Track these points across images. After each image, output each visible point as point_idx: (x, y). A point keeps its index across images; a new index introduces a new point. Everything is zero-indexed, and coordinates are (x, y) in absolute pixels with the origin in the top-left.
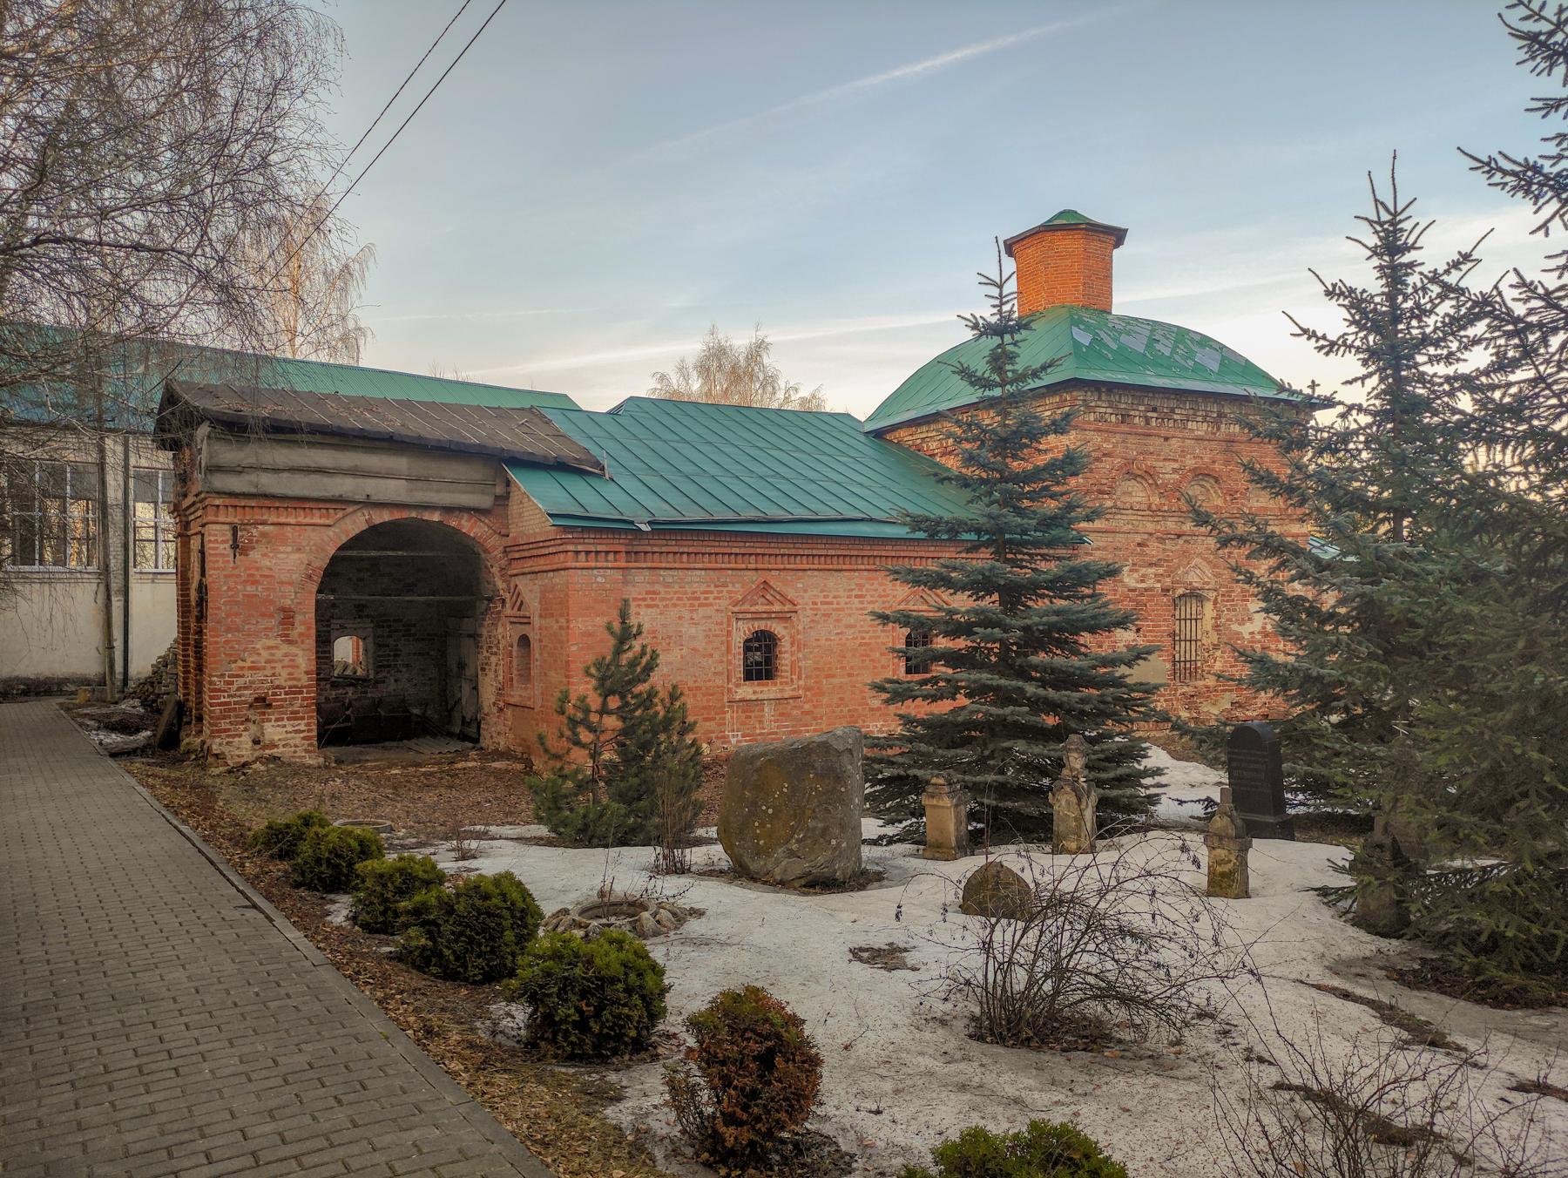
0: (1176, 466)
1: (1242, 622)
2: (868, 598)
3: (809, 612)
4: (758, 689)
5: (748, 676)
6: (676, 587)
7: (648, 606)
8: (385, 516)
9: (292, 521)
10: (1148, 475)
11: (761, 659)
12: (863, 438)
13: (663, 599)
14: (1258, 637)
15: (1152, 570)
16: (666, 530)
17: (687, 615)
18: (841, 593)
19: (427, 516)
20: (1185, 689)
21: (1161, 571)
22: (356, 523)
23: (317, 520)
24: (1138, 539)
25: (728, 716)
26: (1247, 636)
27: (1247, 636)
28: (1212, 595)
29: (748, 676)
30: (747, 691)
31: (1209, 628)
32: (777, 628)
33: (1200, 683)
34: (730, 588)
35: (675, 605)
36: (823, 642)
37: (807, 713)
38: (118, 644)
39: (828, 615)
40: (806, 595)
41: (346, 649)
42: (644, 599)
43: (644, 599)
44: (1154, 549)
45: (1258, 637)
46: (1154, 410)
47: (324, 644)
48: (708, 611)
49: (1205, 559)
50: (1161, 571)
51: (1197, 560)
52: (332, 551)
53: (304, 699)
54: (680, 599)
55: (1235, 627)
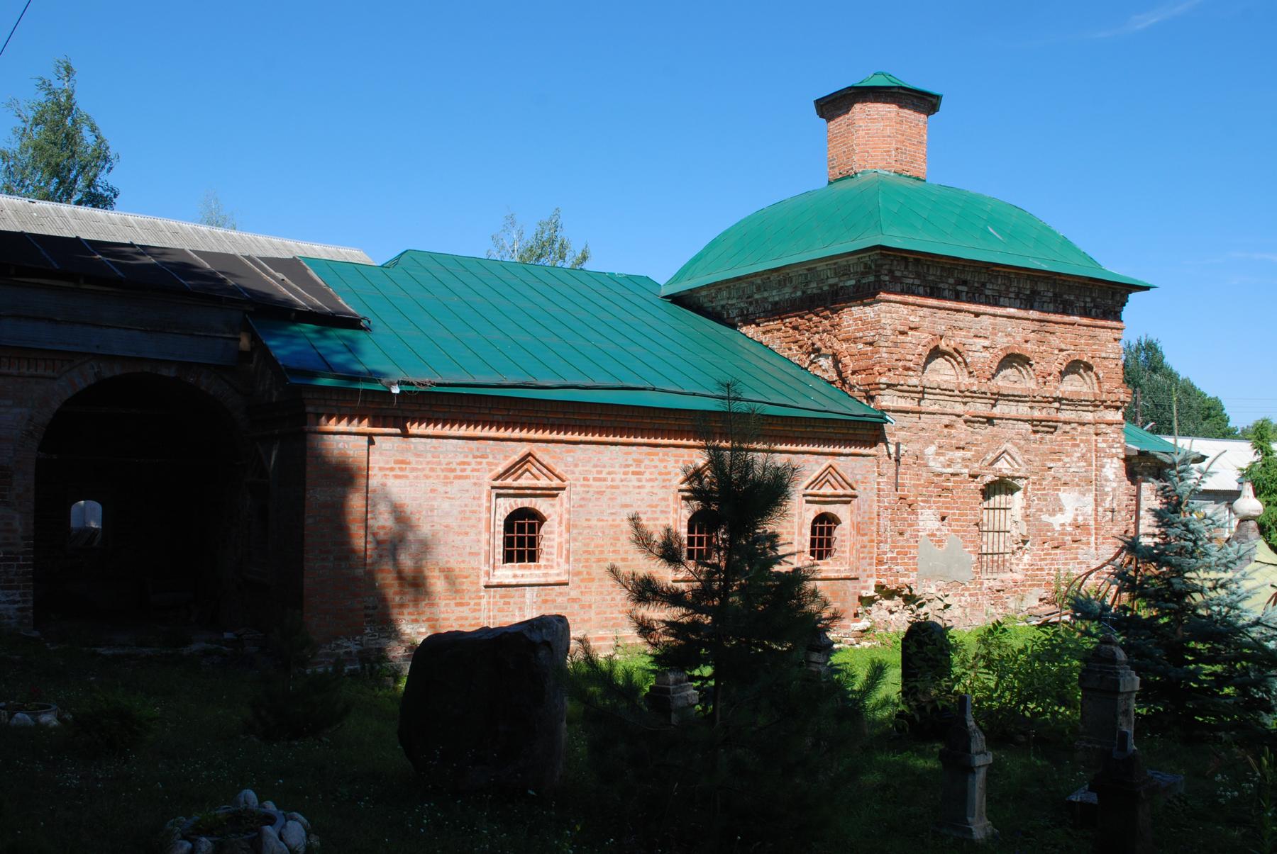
0: (987, 343)
1: (1053, 513)
2: (647, 476)
3: (579, 489)
4: (519, 572)
5: (508, 558)
6: (429, 458)
7: (396, 477)
8: (118, 370)
9: (13, 371)
10: (954, 355)
11: (522, 536)
12: (660, 303)
13: (413, 470)
14: (1069, 529)
15: (960, 454)
16: (907, 412)
17: (441, 489)
18: (617, 469)
19: (165, 372)
20: (992, 583)
21: (969, 454)
22: (82, 378)
23: (40, 372)
24: (946, 420)
25: (484, 601)
26: (1058, 528)
27: (1058, 528)
28: (1021, 483)
29: (508, 558)
30: (509, 573)
31: (1018, 518)
32: (541, 505)
33: (1008, 576)
34: (490, 459)
35: (427, 477)
36: (593, 522)
37: (574, 600)
38: (511, 491)
39: (601, 493)
40: (577, 470)
41: (88, 514)
42: (392, 469)
43: (392, 469)
44: (962, 431)
45: (1069, 529)
46: (965, 283)
47: (50, 512)
48: (466, 484)
49: (1015, 444)
50: (969, 454)
51: (1008, 446)
52: (56, 405)
53: (20, 567)
54: (432, 470)
55: (1045, 518)
